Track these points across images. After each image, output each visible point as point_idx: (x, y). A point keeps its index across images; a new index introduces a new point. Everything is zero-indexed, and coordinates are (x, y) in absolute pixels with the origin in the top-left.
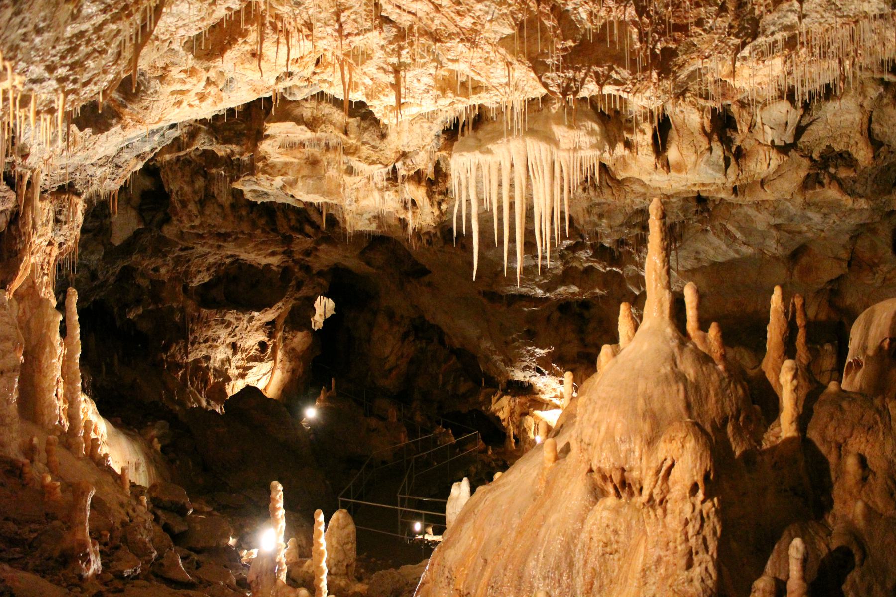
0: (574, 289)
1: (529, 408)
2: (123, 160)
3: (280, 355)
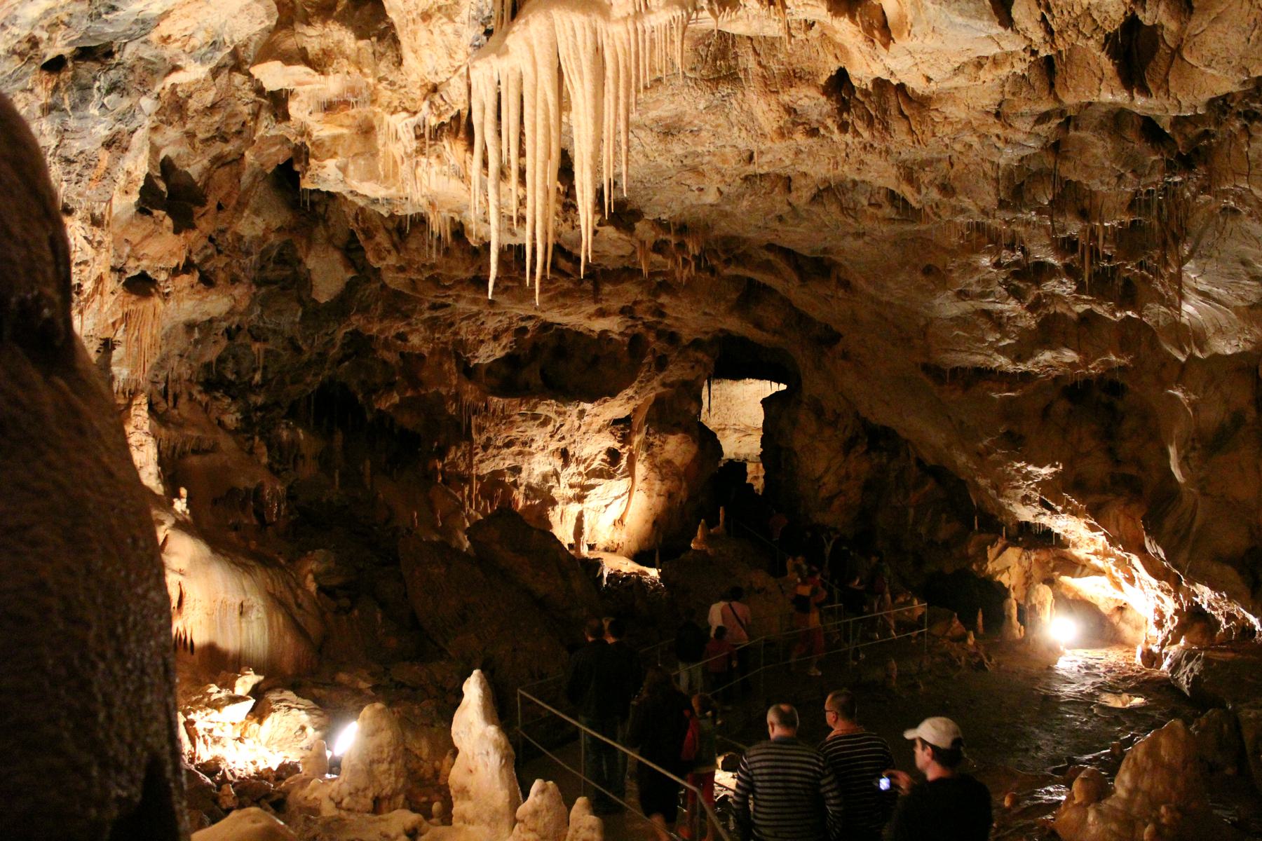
0: (1070, 356)
1: (1053, 570)
2: (75, 152)
3: (641, 469)
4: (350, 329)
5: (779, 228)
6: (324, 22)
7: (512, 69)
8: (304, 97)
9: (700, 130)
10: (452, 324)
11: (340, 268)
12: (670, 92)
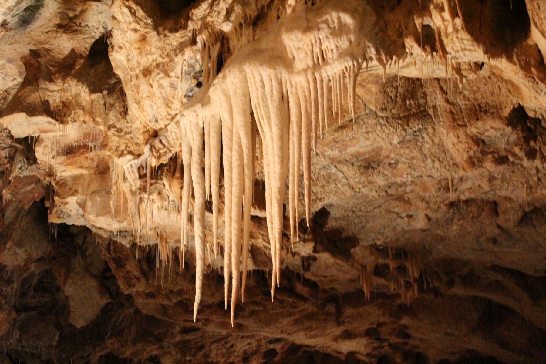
4: (105, 352)
5: (495, 249)
6: (64, 79)
7: (213, 116)
8: (48, 143)
9: (397, 163)
10: (202, 347)
11: (96, 295)
12: (364, 130)
